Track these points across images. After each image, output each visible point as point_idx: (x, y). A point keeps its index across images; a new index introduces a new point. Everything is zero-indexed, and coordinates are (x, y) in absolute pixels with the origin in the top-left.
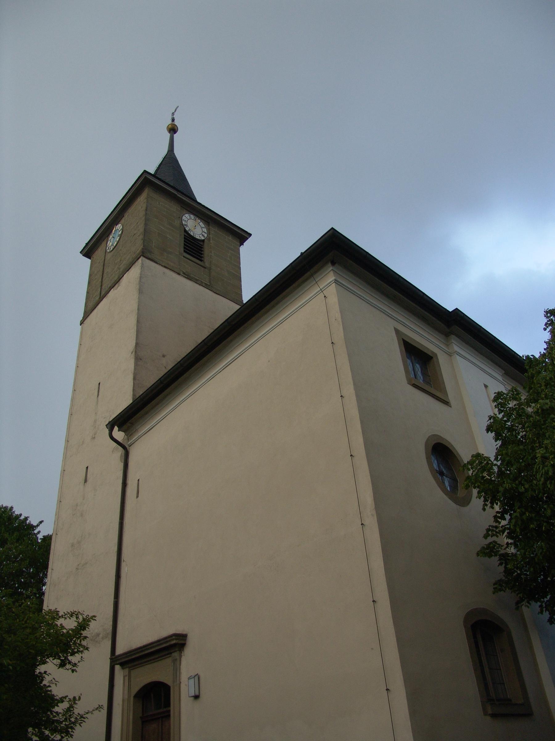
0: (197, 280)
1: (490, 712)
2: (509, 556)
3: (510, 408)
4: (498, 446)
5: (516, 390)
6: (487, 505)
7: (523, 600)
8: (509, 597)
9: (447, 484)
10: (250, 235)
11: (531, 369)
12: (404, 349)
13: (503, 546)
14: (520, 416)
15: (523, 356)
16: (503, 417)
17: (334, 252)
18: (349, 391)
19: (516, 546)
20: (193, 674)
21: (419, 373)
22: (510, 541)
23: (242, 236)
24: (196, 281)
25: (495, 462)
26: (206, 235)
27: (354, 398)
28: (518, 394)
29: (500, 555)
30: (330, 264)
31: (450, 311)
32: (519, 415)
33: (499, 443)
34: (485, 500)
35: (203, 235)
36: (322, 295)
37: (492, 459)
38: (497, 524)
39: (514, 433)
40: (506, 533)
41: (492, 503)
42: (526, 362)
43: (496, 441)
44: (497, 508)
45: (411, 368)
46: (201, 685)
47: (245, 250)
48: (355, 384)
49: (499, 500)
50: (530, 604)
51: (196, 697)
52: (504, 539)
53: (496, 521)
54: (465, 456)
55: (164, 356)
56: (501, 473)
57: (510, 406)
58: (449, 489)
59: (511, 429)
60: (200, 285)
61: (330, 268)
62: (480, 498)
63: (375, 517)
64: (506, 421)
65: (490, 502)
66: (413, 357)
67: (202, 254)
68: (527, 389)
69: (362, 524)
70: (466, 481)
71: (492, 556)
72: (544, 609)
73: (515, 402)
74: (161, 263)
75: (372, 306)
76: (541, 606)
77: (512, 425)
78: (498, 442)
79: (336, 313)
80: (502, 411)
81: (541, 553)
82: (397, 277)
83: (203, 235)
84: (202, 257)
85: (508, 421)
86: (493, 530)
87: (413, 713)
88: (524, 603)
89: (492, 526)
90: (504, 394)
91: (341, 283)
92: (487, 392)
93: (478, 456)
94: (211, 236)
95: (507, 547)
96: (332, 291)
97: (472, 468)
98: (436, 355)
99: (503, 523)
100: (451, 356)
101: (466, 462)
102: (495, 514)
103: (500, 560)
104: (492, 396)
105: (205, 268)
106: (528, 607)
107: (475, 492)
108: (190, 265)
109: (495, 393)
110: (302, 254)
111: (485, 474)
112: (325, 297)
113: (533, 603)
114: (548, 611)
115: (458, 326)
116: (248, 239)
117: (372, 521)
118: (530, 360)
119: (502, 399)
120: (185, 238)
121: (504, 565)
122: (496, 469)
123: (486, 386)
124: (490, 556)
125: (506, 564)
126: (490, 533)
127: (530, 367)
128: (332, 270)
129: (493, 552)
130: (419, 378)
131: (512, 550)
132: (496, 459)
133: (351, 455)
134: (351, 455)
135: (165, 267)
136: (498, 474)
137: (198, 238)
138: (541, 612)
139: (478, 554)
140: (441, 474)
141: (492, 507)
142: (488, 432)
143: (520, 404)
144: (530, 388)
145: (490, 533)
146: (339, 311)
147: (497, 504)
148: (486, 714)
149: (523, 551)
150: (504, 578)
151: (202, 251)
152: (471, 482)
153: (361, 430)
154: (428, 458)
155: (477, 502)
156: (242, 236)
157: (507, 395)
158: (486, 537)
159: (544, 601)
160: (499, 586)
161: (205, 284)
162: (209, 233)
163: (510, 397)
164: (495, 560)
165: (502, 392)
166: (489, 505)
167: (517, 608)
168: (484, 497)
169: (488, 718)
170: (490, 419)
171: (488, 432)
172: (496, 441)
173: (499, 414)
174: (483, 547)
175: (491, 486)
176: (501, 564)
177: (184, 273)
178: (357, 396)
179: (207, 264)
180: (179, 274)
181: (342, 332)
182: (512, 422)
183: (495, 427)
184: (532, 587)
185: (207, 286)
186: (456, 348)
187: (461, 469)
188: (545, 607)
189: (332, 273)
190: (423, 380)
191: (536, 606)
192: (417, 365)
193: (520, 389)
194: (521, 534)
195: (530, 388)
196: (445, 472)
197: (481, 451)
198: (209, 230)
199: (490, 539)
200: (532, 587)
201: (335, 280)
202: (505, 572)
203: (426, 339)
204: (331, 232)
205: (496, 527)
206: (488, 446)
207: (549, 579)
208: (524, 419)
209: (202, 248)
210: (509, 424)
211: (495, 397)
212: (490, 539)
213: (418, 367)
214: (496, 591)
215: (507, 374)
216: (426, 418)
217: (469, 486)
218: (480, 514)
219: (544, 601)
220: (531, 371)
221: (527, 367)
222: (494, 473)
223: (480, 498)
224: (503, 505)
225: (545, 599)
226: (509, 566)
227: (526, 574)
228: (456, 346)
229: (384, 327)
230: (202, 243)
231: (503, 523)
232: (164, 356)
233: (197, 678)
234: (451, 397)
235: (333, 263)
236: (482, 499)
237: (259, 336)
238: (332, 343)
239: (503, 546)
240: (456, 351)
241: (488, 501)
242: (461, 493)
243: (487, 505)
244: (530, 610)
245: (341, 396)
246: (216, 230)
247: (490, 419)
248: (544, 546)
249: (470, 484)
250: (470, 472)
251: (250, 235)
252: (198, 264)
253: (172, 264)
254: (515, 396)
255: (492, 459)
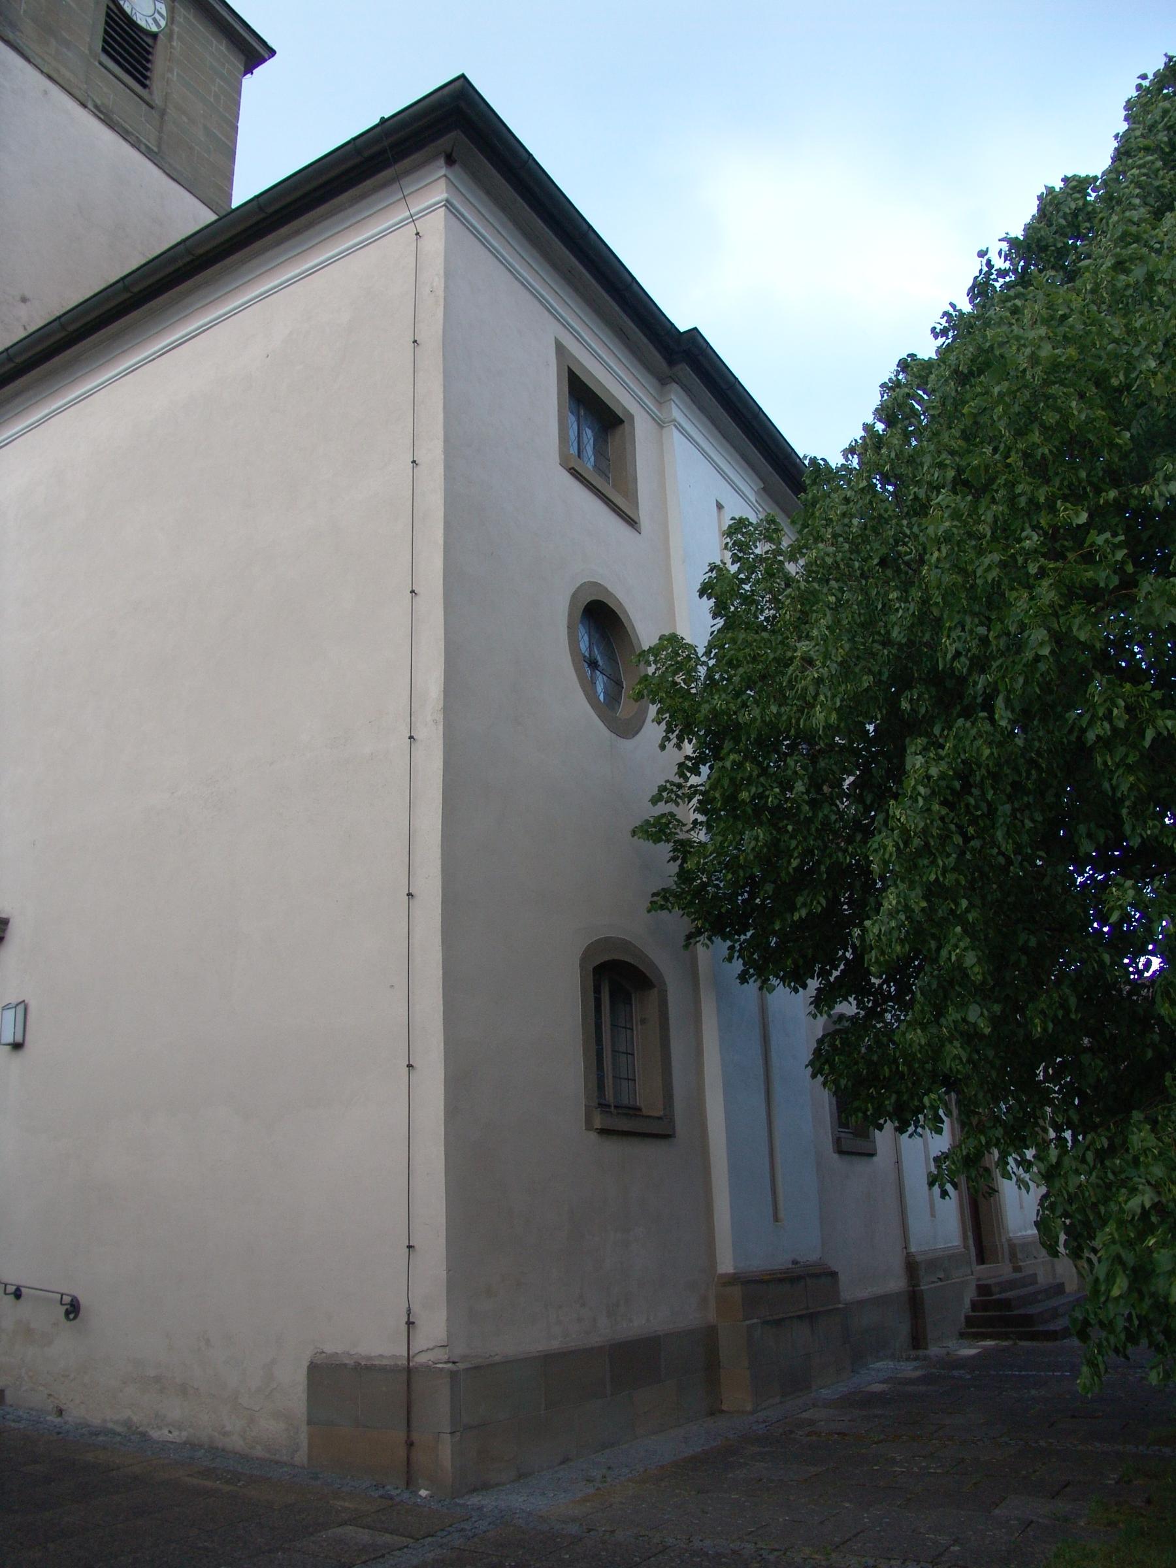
0: (127, 132)
1: (598, 1125)
2: (692, 847)
3: (757, 556)
4: (716, 628)
5: (773, 521)
6: (669, 740)
7: (701, 934)
8: (677, 922)
9: (600, 688)
10: (272, 53)
11: (815, 487)
12: (566, 389)
13: (684, 825)
14: (772, 575)
15: (805, 457)
16: (740, 571)
17: (452, 131)
18: (433, 452)
19: (709, 828)
20: (14, 1001)
21: (589, 450)
22: (701, 818)
23: (252, 51)
24: (125, 134)
25: (704, 659)
26: (163, 23)
27: (440, 470)
28: (777, 530)
29: (675, 842)
30: (442, 162)
31: (682, 330)
32: (770, 575)
33: (720, 622)
34: (669, 730)
35: (155, 20)
36: (411, 229)
37: (701, 651)
38: (681, 781)
39: (753, 608)
40: (695, 801)
41: (680, 739)
42: (808, 471)
43: (714, 618)
44: (688, 749)
45: (573, 434)
46: (28, 1028)
47: (255, 85)
48: (446, 440)
49: (695, 734)
50: (712, 942)
51: (17, 1046)
52: (689, 812)
53: (681, 774)
54: (646, 634)
55: (24, 300)
56: (711, 684)
57: (758, 551)
58: (602, 698)
59: (748, 600)
60: (133, 145)
61: (440, 170)
62: (659, 723)
63: (441, 727)
64: (742, 581)
65: (677, 737)
66: (582, 412)
67: (147, 69)
68: (798, 526)
69: (411, 737)
70: (640, 683)
71: (660, 840)
72: (736, 954)
73: (768, 546)
74: (38, 61)
75: (517, 278)
76: (731, 948)
77: (752, 591)
78: (718, 620)
79: (434, 276)
80: (740, 559)
81: (753, 849)
82: (585, 227)
83: (155, 20)
84: (146, 77)
85: (746, 581)
86: (672, 791)
87: (453, 1110)
88: (701, 938)
89: (672, 783)
90: (751, 524)
91: (457, 210)
92: (719, 516)
93: (673, 641)
94: (176, 29)
95: (692, 829)
96: (436, 224)
97: (655, 662)
98: (631, 417)
99: (694, 780)
100: (662, 427)
101: (646, 648)
102: (682, 760)
103: (674, 850)
104: (728, 522)
105: (152, 107)
106: (708, 947)
107: (653, 710)
108: (112, 85)
109: (733, 518)
110: (383, 121)
111: (679, 678)
112: (417, 234)
113: (718, 940)
114: (743, 959)
115: (688, 364)
116: (265, 60)
117: (431, 734)
118: (819, 470)
119: (743, 534)
120: (108, 15)
121: (679, 862)
122: (702, 671)
123: (720, 507)
124: (657, 840)
125: (684, 861)
126: (665, 794)
127: (814, 483)
128: (445, 176)
129: (665, 834)
130: (586, 460)
131: (702, 836)
132: (707, 653)
133: (412, 592)
134: (412, 592)
135: (50, 77)
136: (706, 686)
137: (142, 23)
138: (730, 959)
139: (634, 833)
140: (593, 664)
141: (679, 746)
142: (701, 596)
143: (778, 552)
144: (805, 526)
145: (665, 794)
146: (442, 273)
147: (690, 742)
148: (589, 1126)
149: (719, 838)
150: (674, 887)
151: (148, 61)
152: (650, 690)
153: (441, 542)
154: (571, 628)
155: (653, 731)
156: (252, 51)
157: (756, 529)
158: (655, 800)
159: (739, 940)
160: (662, 900)
161: (147, 147)
162: (171, 19)
163: (760, 534)
164: (664, 849)
165: (747, 519)
166: (675, 741)
167: (687, 946)
168: (668, 723)
169: (593, 1136)
170: (711, 570)
171: (701, 596)
172: (714, 618)
173: (733, 564)
174: (647, 821)
175: (686, 704)
176: (674, 859)
177: (96, 107)
178: (448, 467)
179: (157, 100)
180: (84, 106)
181: (441, 321)
182: (754, 585)
183: (717, 588)
184: (723, 910)
185: (149, 154)
186: (676, 414)
187: (634, 659)
188: (739, 951)
189: (442, 183)
190: (596, 466)
191: (722, 946)
192: (589, 432)
193: (783, 522)
194: (721, 806)
195: (805, 526)
196: (600, 663)
197: (680, 633)
198: (171, 11)
199: (662, 808)
200: (723, 910)
201: (447, 201)
202: (679, 875)
203: (617, 378)
204: (457, 84)
205: (679, 786)
206: (697, 625)
207: (758, 901)
208: (779, 583)
209: (149, 53)
210: (747, 587)
211: (730, 526)
212: (662, 808)
213: (588, 434)
214: (653, 907)
215: (767, 490)
216: (583, 543)
217: (643, 697)
218: (654, 755)
219: (739, 940)
220: (813, 491)
221: (808, 482)
222: (696, 680)
223: (659, 723)
224: (702, 744)
225: (743, 937)
226: (688, 865)
227: (717, 886)
228: (678, 410)
229: (535, 333)
230: (150, 41)
231: (694, 780)
232: (24, 300)
233: (21, 1008)
234: (645, 512)
235: (450, 161)
236: (663, 725)
237: (253, 295)
238: (415, 341)
239: (684, 825)
240: (675, 420)
241: (673, 732)
242: (626, 708)
243: (669, 740)
244: (712, 954)
245: (414, 462)
246: (191, 17)
247: (711, 570)
248: (761, 836)
249: (645, 692)
250: (651, 670)
251: (272, 53)
252: (136, 94)
253: (68, 74)
254: (770, 531)
255: (701, 651)
